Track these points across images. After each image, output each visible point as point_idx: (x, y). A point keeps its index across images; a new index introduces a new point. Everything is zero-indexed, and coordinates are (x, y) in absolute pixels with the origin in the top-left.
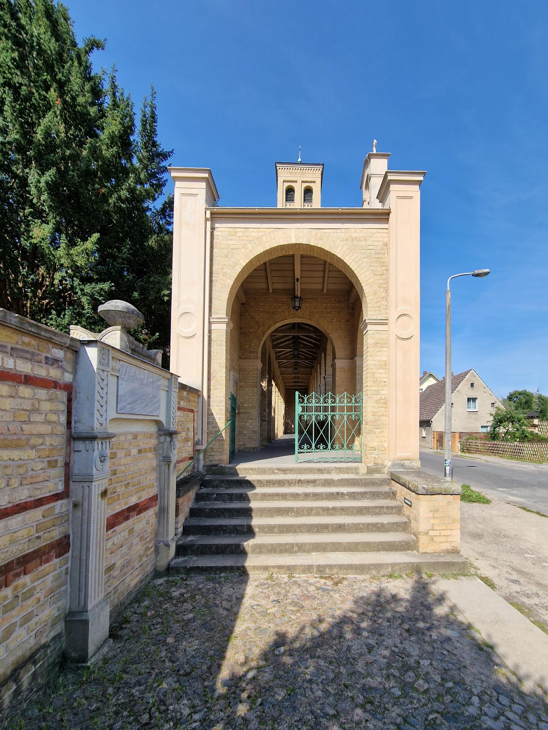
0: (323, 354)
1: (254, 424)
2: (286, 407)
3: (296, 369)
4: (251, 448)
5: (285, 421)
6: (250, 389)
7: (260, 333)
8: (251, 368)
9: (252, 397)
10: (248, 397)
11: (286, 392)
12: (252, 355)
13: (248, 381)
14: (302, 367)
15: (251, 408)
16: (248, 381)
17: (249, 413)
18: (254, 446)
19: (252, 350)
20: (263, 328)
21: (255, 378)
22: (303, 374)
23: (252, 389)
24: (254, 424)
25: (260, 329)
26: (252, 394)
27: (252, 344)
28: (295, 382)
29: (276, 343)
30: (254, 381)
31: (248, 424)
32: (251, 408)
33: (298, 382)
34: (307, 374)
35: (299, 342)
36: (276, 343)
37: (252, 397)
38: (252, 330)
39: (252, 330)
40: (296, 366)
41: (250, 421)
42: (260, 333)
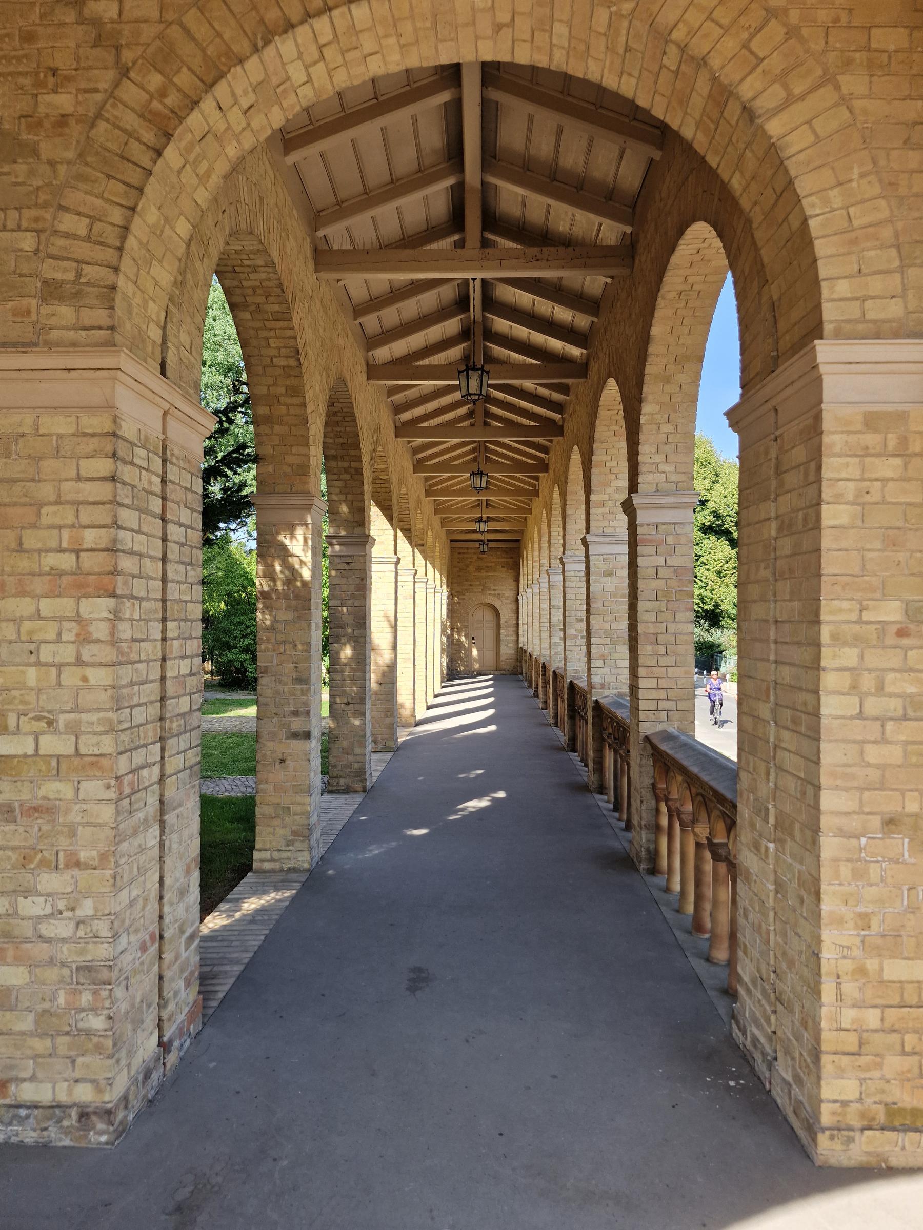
0: (612, 389)
1: (87, 908)
2: (451, 596)
3: (480, 473)
4: (57, 1109)
5: (450, 638)
6: (47, 606)
7: (130, 120)
8: (61, 425)
9: (70, 677)
10: (32, 675)
11: (452, 550)
12: (65, 313)
13: (31, 540)
14: (501, 467)
15: (58, 767)
16: (31, 540)
17: (42, 810)
18: (85, 1094)
19: (63, 273)
20: (155, 80)
21: (101, 515)
22: (508, 492)
23: (66, 605)
24: (87, 908)
25: (130, 92)
26: (67, 653)
27: (68, 223)
28: (480, 520)
29: (407, 416)
30: (90, 537)
31: (32, 907)
32: (58, 767)
33: (489, 519)
34: (519, 492)
35: (487, 414)
36: (407, 416)
37: (70, 677)
38: (64, 101)
39: (64, 101)
40: (480, 462)
41: (49, 881)
42: (130, 120)
